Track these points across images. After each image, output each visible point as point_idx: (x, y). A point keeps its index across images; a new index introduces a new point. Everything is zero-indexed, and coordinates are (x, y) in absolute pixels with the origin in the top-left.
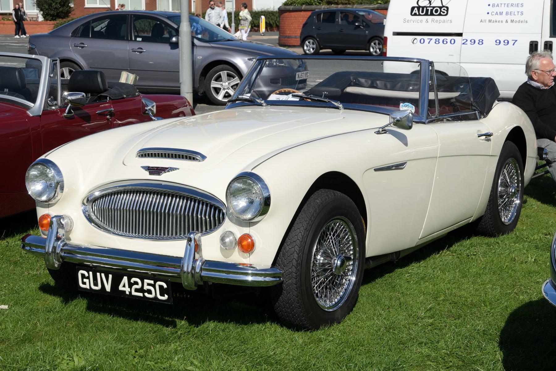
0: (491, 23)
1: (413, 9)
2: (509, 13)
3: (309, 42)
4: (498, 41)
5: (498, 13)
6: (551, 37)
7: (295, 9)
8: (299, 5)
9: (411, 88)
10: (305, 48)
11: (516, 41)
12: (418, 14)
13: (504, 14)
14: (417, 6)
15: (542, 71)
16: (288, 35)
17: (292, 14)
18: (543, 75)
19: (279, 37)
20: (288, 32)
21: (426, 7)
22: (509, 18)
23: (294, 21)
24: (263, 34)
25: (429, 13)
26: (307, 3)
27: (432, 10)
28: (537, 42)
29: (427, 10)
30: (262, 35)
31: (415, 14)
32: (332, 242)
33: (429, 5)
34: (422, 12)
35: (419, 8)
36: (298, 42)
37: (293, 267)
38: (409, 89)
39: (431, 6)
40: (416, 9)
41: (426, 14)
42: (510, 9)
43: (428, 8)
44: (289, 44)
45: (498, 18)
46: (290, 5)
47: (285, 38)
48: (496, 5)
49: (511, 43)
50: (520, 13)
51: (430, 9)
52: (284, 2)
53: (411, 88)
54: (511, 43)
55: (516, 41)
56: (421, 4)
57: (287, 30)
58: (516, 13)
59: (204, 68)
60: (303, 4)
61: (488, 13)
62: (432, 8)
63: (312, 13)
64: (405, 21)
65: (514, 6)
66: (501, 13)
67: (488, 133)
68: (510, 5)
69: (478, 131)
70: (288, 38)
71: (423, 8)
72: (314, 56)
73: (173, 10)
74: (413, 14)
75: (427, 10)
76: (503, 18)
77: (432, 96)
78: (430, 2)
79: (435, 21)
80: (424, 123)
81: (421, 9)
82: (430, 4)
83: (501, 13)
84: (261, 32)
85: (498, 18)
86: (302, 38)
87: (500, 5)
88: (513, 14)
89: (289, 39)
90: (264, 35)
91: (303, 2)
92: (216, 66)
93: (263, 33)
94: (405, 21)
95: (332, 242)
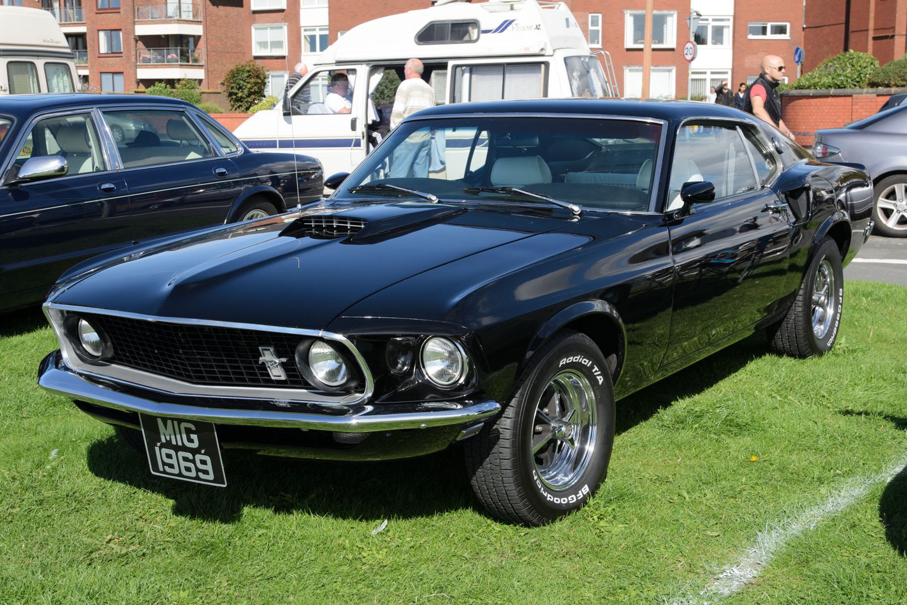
16: (802, 131)
17: (812, 101)
20: (804, 127)
23: (814, 111)
26: (837, 85)
46: (806, 89)
57: (802, 124)
70: (804, 135)
89: (804, 137)
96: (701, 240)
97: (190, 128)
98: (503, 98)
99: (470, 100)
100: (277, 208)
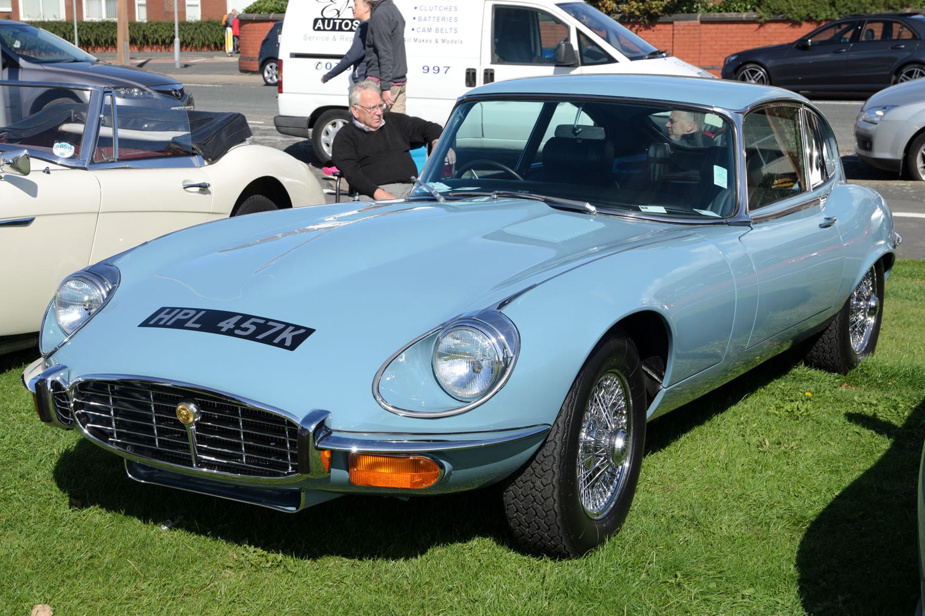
0: (445, 44)
1: (316, 21)
2: (440, 30)
3: (271, 67)
4: (426, 68)
5: (426, 30)
6: (493, 62)
7: (259, 19)
8: (265, 13)
9: (146, 126)
10: (266, 75)
11: (449, 68)
12: (322, 28)
13: (434, 30)
14: (322, 17)
15: (362, 107)
16: (250, 56)
17: (256, 25)
18: (364, 113)
19: (239, 59)
20: (252, 52)
21: (334, 19)
22: (440, 36)
23: (258, 36)
24: (229, 55)
25: (337, 28)
26: (277, 9)
27: (340, 24)
28: (475, 70)
29: (335, 24)
30: (228, 56)
31: (319, 29)
32: (600, 400)
33: (336, 17)
34: (328, 26)
35: (323, 20)
36: (256, 66)
37: (553, 442)
38: (143, 127)
39: (340, 17)
40: (320, 21)
41: (334, 29)
42: (441, 24)
43: (335, 21)
44: (252, 69)
45: (425, 36)
46: (252, 13)
47: (247, 60)
48: (423, 19)
49: (442, 70)
50: (453, 30)
51: (338, 22)
52: (245, 8)
53: (146, 126)
54: (442, 70)
55: (449, 68)
56: (327, 15)
57: (250, 49)
58: (448, 30)
59: (35, 101)
60: (272, 11)
61: (413, 30)
62: (341, 21)
63: (275, 25)
64: (306, 38)
65: (446, 20)
66: (430, 30)
67: (204, 183)
68: (441, 19)
69: (184, 181)
70: (252, 60)
71: (329, 20)
72: (133, 85)
73: (107, 17)
74: (316, 28)
75: (335, 24)
76: (433, 36)
77: (106, 131)
78: (338, 12)
79: (345, 39)
80: (85, 169)
81: (326, 21)
82: (339, 16)
83: (430, 30)
84: (227, 52)
85: (425, 36)
86: (261, 60)
87: (428, 19)
88: (444, 31)
89: (252, 62)
90: (232, 56)
91: (271, 8)
92: (64, 97)
93: (230, 53)
94: (306, 38)
95: (600, 400)
96: (762, 174)
97: (77, 22)
98: (197, 6)
99: (189, 6)
100: (66, 97)
